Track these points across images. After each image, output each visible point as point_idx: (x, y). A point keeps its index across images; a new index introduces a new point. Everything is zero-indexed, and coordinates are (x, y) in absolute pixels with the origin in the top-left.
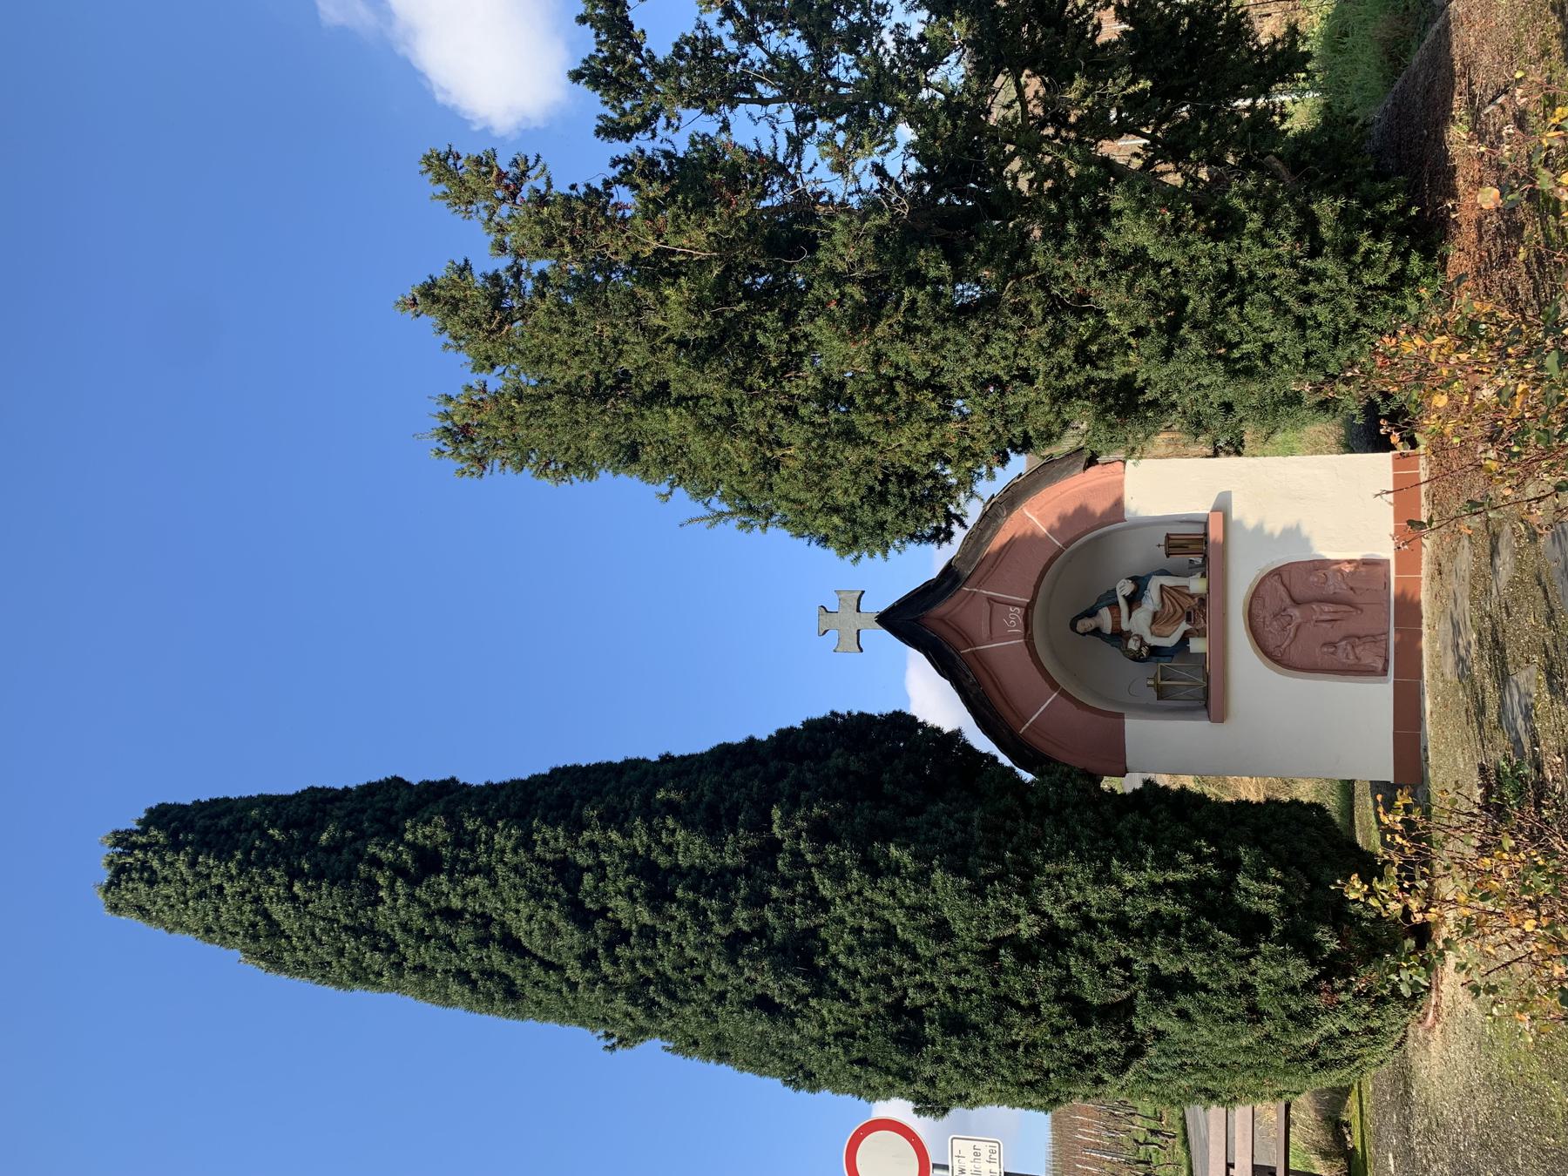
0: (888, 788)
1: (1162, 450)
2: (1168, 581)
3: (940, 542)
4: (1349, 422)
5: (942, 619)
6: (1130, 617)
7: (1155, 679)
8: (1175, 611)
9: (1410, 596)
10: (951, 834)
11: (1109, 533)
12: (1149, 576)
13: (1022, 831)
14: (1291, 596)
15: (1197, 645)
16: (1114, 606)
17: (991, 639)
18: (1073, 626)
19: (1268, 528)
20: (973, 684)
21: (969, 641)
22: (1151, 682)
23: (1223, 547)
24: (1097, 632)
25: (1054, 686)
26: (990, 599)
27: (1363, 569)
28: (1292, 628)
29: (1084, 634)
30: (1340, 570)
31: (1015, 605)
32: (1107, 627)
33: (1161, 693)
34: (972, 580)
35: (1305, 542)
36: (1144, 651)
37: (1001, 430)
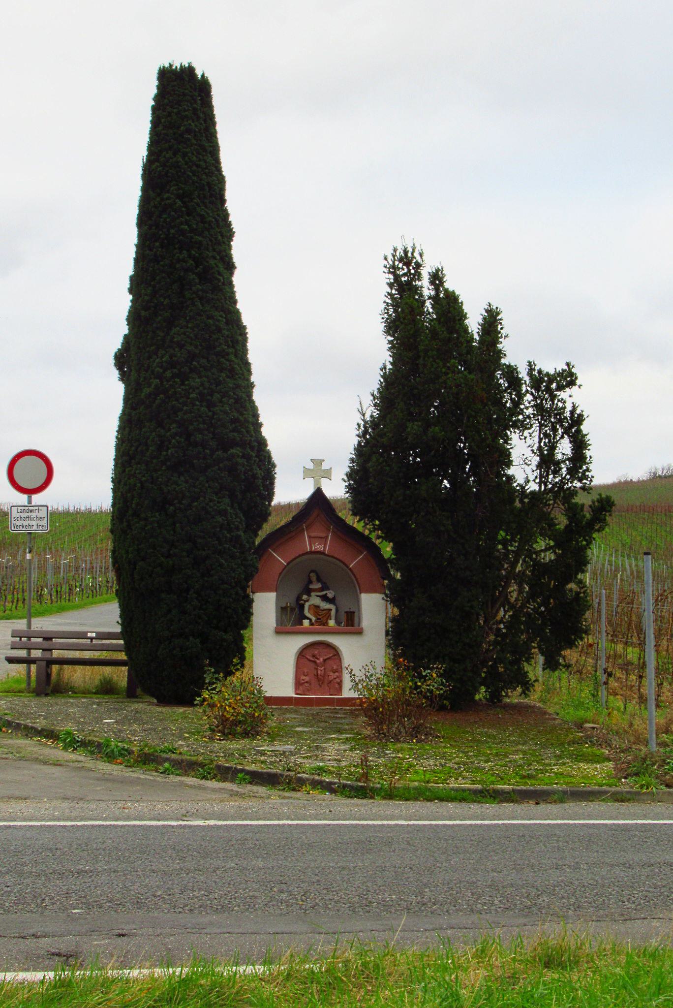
0: (249, 495)
1: (390, 610)
2: (333, 613)
6: (317, 596)
11: (355, 587)
15: (306, 623)
16: (322, 590)
17: (309, 537)
18: (312, 571)
24: (310, 582)
26: (327, 537)
32: (311, 587)
36: (302, 602)
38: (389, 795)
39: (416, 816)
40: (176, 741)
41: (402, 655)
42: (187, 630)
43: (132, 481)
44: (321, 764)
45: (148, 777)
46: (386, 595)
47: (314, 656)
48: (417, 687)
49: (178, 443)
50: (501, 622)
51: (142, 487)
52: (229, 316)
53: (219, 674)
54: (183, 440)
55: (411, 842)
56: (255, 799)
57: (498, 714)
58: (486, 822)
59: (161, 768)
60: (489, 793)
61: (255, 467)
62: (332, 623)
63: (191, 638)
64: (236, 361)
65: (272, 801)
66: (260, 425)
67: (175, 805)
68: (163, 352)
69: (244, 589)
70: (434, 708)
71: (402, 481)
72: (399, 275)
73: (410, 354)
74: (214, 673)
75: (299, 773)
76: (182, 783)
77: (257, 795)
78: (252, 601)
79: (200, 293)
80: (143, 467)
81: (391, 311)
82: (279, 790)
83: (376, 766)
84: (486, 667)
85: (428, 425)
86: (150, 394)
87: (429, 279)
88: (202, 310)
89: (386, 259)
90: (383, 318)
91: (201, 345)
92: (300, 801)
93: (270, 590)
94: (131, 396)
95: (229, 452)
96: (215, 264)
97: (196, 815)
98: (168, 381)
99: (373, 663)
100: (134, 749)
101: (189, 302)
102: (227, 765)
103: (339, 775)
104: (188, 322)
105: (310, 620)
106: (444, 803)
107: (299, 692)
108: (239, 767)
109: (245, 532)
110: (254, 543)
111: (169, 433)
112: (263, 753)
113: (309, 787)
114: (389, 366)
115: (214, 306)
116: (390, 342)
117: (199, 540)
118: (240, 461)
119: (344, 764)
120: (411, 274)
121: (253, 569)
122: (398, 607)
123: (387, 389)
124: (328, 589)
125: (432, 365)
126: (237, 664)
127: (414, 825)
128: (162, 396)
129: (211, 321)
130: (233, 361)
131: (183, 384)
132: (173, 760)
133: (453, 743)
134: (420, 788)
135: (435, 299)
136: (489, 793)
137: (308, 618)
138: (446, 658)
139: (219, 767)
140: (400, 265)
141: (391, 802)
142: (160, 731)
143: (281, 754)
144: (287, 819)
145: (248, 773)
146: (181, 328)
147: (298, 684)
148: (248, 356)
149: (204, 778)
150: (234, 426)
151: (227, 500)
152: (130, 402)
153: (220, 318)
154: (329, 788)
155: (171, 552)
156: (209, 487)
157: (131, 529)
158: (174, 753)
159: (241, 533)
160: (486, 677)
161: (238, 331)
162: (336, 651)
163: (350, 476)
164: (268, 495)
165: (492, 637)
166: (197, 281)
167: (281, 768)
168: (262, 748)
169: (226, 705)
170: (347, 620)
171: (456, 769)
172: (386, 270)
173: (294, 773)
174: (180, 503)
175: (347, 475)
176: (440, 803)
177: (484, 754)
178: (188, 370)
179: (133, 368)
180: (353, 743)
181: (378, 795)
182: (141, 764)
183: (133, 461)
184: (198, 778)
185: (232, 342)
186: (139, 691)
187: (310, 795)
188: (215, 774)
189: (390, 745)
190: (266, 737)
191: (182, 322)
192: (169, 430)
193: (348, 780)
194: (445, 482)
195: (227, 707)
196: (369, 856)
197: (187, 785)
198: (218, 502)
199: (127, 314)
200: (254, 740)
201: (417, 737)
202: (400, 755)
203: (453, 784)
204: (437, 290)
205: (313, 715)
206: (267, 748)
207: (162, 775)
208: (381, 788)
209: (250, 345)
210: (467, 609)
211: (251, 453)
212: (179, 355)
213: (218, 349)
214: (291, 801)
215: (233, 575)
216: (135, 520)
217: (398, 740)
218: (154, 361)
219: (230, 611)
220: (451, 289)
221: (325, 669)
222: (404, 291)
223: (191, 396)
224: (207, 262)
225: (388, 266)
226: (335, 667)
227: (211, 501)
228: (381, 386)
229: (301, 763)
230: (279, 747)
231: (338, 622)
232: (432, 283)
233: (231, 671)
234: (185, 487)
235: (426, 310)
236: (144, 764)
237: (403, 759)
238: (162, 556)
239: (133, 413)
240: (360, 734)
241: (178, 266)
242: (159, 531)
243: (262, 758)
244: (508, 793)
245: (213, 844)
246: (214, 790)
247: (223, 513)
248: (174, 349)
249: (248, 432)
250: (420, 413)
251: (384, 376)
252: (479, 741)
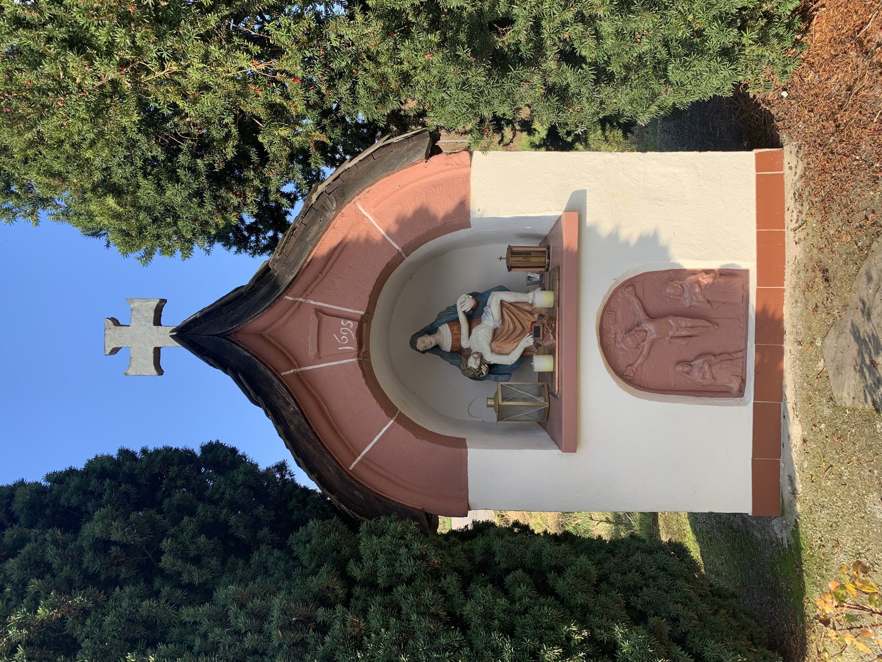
2: (508, 297)
5: (260, 335)
6: (497, 393)
7: (495, 398)
8: (515, 328)
9: (771, 312)
10: (238, 634)
11: (553, 252)
13: (337, 626)
14: (645, 310)
17: (319, 358)
18: (413, 344)
19: (624, 233)
20: (295, 413)
21: (292, 360)
22: (491, 402)
23: (576, 257)
24: (436, 349)
25: (390, 409)
26: (319, 311)
27: (722, 280)
28: (646, 345)
29: (423, 352)
30: (698, 282)
31: (346, 318)
32: (447, 346)
33: (502, 414)
34: (297, 288)
35: (664, 251)
36: (484, 369)
37: (323, 89)
93: (461, 466)
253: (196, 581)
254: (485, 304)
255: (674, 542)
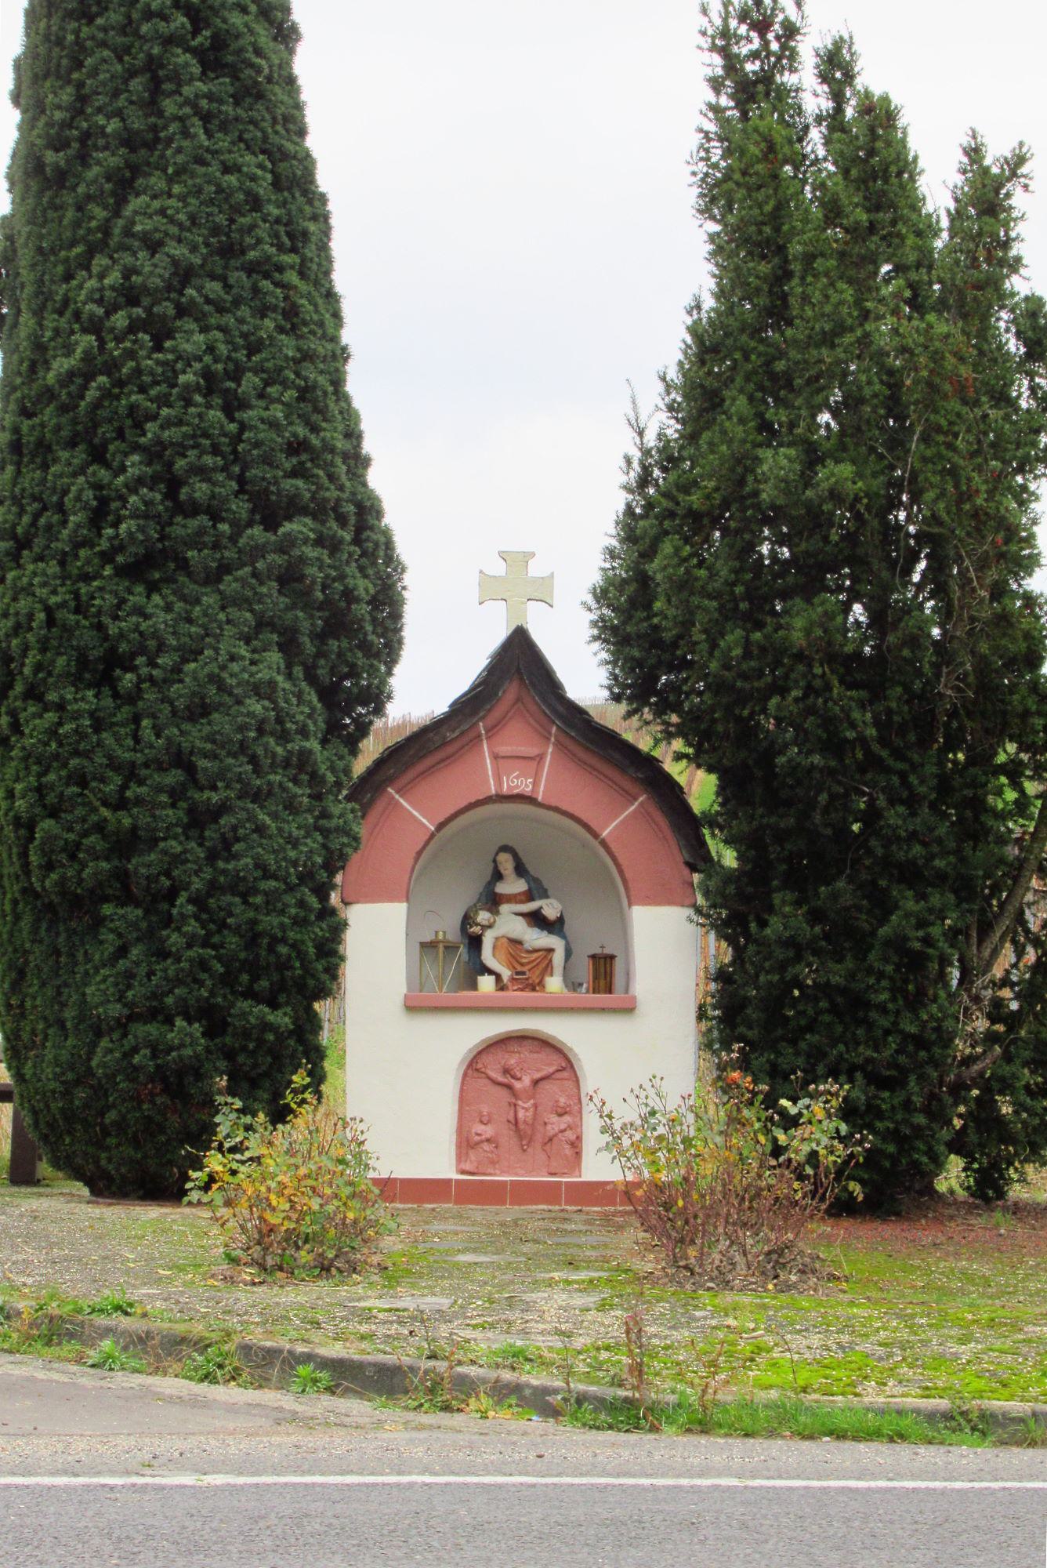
0: (334, 644)
2: (558, 958)
3: (610, 688)
4: (696, 323)
8: (522, 965)
11: (619, 896)
12: (564, 937)
15: (486, 983)
16: (529, 896)
17: (496, 757)
18: (505, 849)
20: (445, 737)
24: (498, 876)
26: (541, 758)
29: (495, 861)
32: (501, 888)
36: (476, 930)
38: (700, 1422)
39: (768, 1470)
40: (134, 1286)
41: (744, 1064)
42: (169, 1000)
43: (23, 604)
44: (519, 1343)
45: (56, 1376)
46: (699, 911)
47: (506, 1071)
48: (777, 1150)
49: (146, 503)
50: (1005, 982)
51: (51, 622)
52: (283, 165)
53: (254, 1115)
54: (158, 497)
55: (751, 1524)
56: (342, 1431)
57: (997, 1226)
58: (958, 1485)
59: (91, 1353)
60: (969, 1421)
61: (351, 569)
62: (554, 983)
63: (179, 1022)
64: (303, 286)
65: (386, 1435)
66: (366, 462)
67: (124, 1442)
68: (106, 261)
69: (322, 892)
70: (823, 1199)
71: (743, 606)
72: (738, 56)
73: (764, 268)
74: (242, 1111)
75: (460, 1363)
76: (147, 1393)
77: (347, 1420)
78: (338, 929)
79: (204, 103)
80: (53, 568)
81: (716, 155)
82: (406, 1408)
83: (666, 1348)
84: (965, 1102)
85: (813, 456)
86: (71, 374)
87: (817, 67)
88: (208, 150)
89: (704, 11)
90: (694, 174)
91: (207, 245)
92: (460, 1436)
93: (392, 898)
94: (18, 381)
95: (281, 530)
96: (246, 25)
97: (178, 1463)
98: (119, 340)
99: (656, 1082)
100: (21, 1305)
101: (173, 128)
102: (268, 1344)
103: (568, 1372)
104: (170, 181)
105: (498, 977)
106: (848, 1445)
107: (467, 1167)
108: (300, 1348)
109: (324, 742)
110: (347, 771)
111: (121, 479)
112: (367, 1316)
113: (486, 1402)
114: (709, 303)
115: (241, 139)
116: (712, 238)
117: (203, 763)
118: (311, 552)
119: (579, 1342)
120: (769, 54)
121: (345, 840)
122: (731, 940)
123: (703, 362)
124: (544, 894)
125: (827, 297)
126: (305, 1088)
127: (761, 1487)
128: (102, 379)
129: (232, 179)
130: (296, 287)
131: (158, 348)
132: (125, 1333)
133: (874, 1294)
134: (784, 1406)
135: (834, 121)
136: (969, 1421)
137: (490, 972)
138: (858, 1075)
139: (246, 1349)
140: (743, 29)
141: (703, 1440)
142: (95, 1263)
143: (413, 1318)
144: (422, 1473)
145: (326, 1364)
146: (154, 197)
147: (465, 1144)
148: (335, 276)
149: (208, 1377)
150: (294, 460)
151: (275, 657)
152: (18, 394)
153: (259, 172)
154: (541, 1403)
155: (128, 794)
156: (229, 622)
157: (22, 734)
158: (127, 1314)
159: (314, 745)
160: (964, 1127)
161: (308, 209)
162: (569, 1061)
163: (602, 595)
164: (386, 645)
165: (981, 1024)
166: (196, 70)
167: (412, 1351)
168: (362, 1304)
169: (269, 1190)
170: (596, 978)
171: (880, 1359)
172: (705, 43)
173: (445, 1364)
174: (152, 664)
175: (594, 592)
176: (836, 1444)
177: (959, 1322)
178: (171, 311)
179: (23, 306)
180: (607, 1292)
181: (671, 1421)
182: (39, 1346)
183: (26, 553)
184: (191, 1379)
185: (289, 235)
186: (44, 1168)
187: (488, 1423)
188: (236, 1369)
189: (705, 1297)
190: (375, 1278)
191: (157, 181)
192: (123, 469)
193: (592, 1383)
194: (857, 608)
195: (273, 1197)
196: (633, 1551)
197: (160, 1397)
198: (253, 663)
199: (7, 161)
200: (343, 1283)
201: (776, 1277)
202: (731, 1322)
203: (872, 1395)
204: (838, 98)
205: (502, 1224)
206: (379, 1304)
207: (92, 1371)
208: (679, 1405)
209: (340, 245)
210: (917, 945)
211: (340, 532)
212: (147, 269)
213: (252, 255)
214: (436, 1434)
215: (292, 854)
216: (32, 709)
217: (727, 1284)
218: (81, 287)
219: (283, 950)
220: (877, 91)
221: (536, 1106)
222: (752, 98)
223: (182, 379)
224: (225, 21)
225: (710, 32)
226: (562, 1100)
227: (233, 658)
228: (685, 353)
229: (467, 1341)
230: (408, 1302)
231: (572, 985)
232: (824, 78)
233: (287, 1105)
234: (165, 622)
235: (809, 149)
236: (49, 1343)
237: (739, 1332)
238: (105, 804)
239: (26, 425)
240: (626, 1271)
241: (145, 28)
242: (95, 738)
243: (364, 1328)
244: (1021, 1420)
245: (214, 1525)
246: (232, 1409)
247: (264, 691)
248: (134, 254)
249: (331, 477)
250: (792, 425)
251: (693, 330)
252: (944, 1291)
253: (320, 672)
254: (550, 932)
255: (888, 692)
